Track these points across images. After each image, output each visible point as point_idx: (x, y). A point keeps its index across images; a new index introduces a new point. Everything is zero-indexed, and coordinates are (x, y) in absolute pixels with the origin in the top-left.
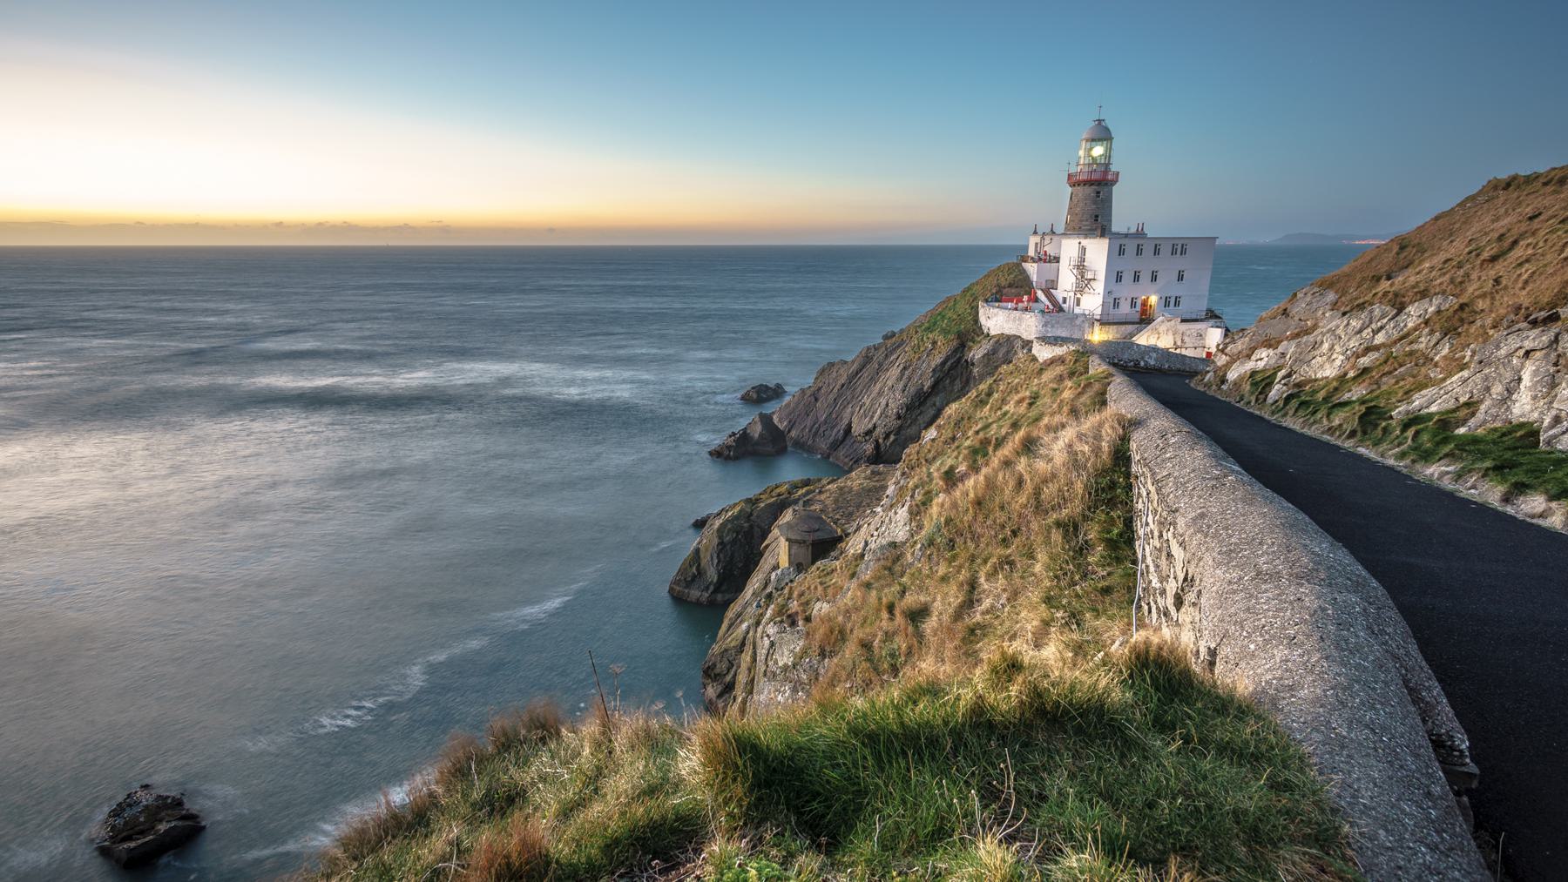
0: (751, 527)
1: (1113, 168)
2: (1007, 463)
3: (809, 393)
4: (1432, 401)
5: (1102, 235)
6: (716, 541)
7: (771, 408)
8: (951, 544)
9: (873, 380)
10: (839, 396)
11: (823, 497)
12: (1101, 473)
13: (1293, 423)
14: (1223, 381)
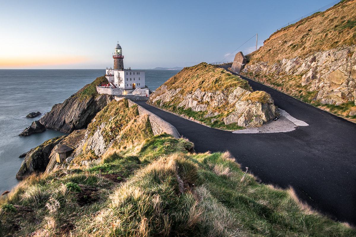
0: (43, 153)
1: (122, 55)
2: (133, 124)
3: (50, 113)
4: (181, 105)
5: (123, 70)
6: (32, 159)
7: (37, 119)
8: (126, 137)
9: (70, 108)
10: (60, 113)
11: (65, 140)
12: (147, 123)
13: (164, 110)
14: (152, 102)
